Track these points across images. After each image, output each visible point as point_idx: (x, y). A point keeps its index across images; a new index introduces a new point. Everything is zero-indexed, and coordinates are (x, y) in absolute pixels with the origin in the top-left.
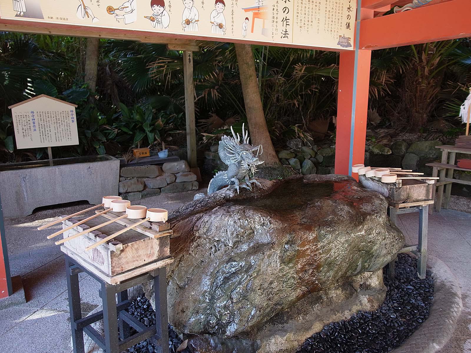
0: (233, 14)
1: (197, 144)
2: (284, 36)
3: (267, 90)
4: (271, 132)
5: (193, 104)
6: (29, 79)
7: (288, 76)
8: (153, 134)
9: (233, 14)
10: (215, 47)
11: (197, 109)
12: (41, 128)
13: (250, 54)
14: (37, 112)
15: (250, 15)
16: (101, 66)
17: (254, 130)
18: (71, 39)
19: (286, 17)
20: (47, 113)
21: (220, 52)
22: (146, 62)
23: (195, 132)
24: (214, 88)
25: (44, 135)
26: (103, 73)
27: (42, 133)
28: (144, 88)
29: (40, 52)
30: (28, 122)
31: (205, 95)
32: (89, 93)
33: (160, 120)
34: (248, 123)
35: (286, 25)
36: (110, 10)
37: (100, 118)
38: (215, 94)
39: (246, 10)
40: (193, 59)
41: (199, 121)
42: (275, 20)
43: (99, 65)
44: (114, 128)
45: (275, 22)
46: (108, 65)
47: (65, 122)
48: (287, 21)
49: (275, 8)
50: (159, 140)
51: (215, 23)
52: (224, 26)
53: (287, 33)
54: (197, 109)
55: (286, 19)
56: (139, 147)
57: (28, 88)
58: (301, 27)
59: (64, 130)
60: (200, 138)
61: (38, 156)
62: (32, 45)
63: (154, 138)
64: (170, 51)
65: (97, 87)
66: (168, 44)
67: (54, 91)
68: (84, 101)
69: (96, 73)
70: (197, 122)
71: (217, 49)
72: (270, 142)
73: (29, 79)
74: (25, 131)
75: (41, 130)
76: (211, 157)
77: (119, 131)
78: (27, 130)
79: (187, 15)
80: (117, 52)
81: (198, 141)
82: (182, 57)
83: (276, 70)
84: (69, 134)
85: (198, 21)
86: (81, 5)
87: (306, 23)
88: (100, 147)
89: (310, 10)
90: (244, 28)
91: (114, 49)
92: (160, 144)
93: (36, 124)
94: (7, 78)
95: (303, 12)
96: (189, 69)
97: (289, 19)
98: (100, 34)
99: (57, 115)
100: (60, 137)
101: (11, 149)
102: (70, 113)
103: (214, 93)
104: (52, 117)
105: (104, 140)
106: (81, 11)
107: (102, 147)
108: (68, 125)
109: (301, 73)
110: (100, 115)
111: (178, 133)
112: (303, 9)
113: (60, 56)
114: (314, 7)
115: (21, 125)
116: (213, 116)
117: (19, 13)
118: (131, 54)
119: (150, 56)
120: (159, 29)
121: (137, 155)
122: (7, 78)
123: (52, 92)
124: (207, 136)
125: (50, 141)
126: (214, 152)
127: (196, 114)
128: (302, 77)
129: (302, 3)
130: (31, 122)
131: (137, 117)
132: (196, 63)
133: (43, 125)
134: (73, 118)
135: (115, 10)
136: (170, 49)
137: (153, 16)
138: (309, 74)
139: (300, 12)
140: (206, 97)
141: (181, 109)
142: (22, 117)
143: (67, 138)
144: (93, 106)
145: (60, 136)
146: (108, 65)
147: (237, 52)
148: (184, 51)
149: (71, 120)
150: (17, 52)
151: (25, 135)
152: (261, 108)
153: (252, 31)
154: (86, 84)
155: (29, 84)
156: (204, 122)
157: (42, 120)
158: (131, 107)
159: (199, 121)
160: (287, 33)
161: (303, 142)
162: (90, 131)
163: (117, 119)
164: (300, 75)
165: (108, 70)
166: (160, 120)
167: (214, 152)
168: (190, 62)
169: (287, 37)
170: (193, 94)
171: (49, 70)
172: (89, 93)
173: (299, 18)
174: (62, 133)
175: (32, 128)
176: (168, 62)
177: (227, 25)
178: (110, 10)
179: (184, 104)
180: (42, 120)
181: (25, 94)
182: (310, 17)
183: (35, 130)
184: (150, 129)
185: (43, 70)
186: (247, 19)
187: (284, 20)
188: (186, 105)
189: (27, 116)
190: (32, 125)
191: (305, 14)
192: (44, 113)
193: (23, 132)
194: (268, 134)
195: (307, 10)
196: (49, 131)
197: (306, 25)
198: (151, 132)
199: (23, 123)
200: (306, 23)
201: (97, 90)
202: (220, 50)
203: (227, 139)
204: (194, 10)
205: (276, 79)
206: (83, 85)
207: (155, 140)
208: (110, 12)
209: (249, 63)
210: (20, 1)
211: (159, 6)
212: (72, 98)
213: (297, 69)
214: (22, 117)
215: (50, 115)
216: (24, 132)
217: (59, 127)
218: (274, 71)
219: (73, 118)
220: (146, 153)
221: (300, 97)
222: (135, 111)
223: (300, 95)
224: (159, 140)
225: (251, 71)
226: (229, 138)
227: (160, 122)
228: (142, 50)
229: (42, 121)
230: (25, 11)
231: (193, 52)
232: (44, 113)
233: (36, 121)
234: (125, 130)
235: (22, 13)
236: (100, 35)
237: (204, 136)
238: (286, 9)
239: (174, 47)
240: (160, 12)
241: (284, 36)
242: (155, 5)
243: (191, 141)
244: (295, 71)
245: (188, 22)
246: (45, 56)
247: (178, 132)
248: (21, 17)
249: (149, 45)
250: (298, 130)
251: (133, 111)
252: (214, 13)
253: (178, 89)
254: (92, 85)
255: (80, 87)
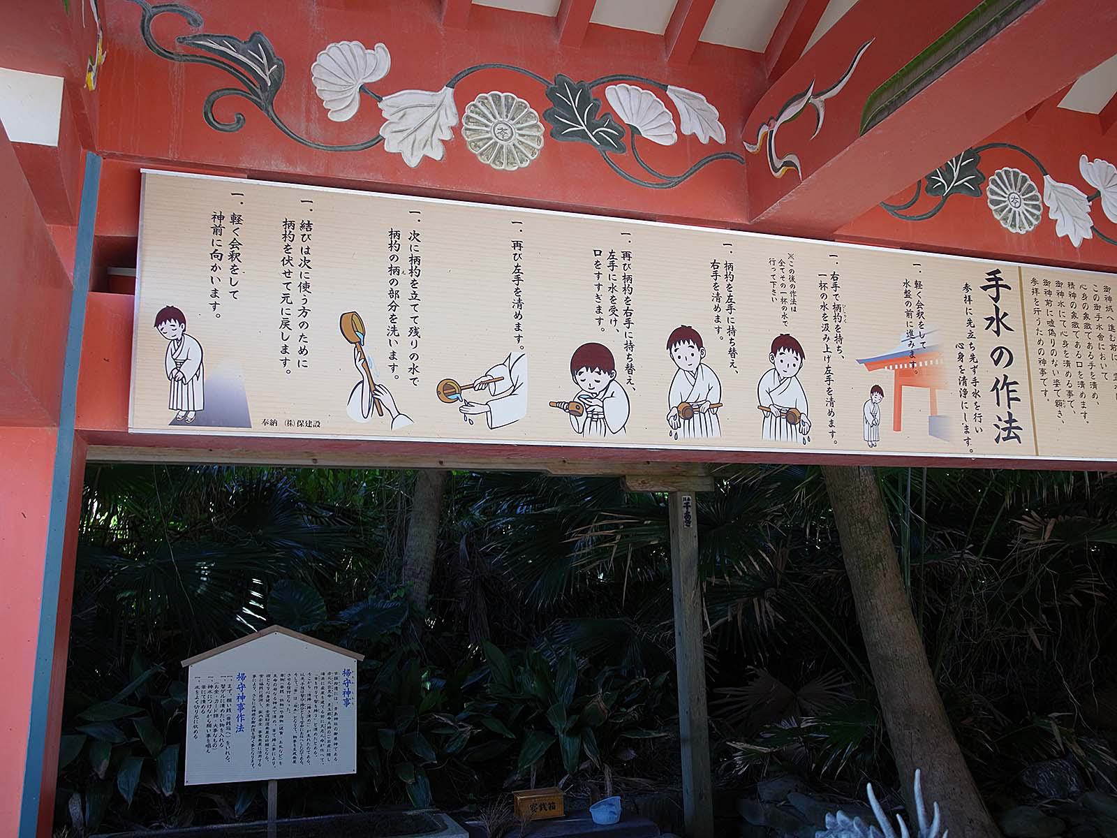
0: (829, 379)
1: (712, 771)
2: (1004, 434)
3: (930, 594)
4: (965, 739)
5: (700, 645)
6: (256, 581)
7: (998, 549)
8: (577, 741)
9: (829, 379)
10: (761, 477)
11: (710, 655)
12: (257, 722)
13: (871, 492)
14: (254, 676)
15: (886, 377)
16: (446, 539)
17: (907, 732)
18: (382, 474)
19: (1006, 377)
20: (279, 678)
21: (776, 489)
22: (566, 527)
23: (706, 733)
24: (760, 593)
25: (263, 743)
26: (450, 557)
27: (257, 738)
28: (560, 596)
29: (300, 510)
30: (226, 703)
31: (735, 617)
32: (407, 613)
33: (599, 699)
34: (880, 708)
35: (1009, 399)
36: (448, 390)
37: (428, 685)
38: (765, 612)
39: (873, 364)
40: (698, 510)
41: (716, 690)
42: (970, 388)
43: (441, 536)
44: (463, 720)
45: (970, 394)
46: (464, 537)
47: (326, 704)
48: (1011, 387)
49: (967, 352)
50: (595, 760)
51: (773, 409)
52: (803, 417)
53: (1014, 424)
54: (710, 655)
55: (1005, 383)
56: (533, 782)
57: (253, 603)
58: (1058, 404)
59: (319, 729)
60: (721, 754)
61: (240, 808)
62: (284, 493)
63: (580, 752)
64: (632, 494)
65: (430, 597)
66: (624, 476)
67: (318, 609)
68: (394, 634)
69: (431, 558)
70: (711, 696)
71: (766, 481)
72: (965, 774)
73: (256, 581)
74: (215, 730)
75: (257, 728)
76: (762, 820)
77: (476, 732)
78: (219, 729)
79: (682, 391)
80: (492, 499)
81: (715, 762)
82: (666, 508)
83: (948, 533)
84: (333, 742)
85: (719, 405)
86: (362, 382)
87: (1076, 390)
88: (416, 783)
89: (1084, 351)
90: (870, 419)
91: (484, 494)
92: (596, 772)
93: (247, 712)
94: (205, 579)
95: (1061, 358)
96: (686, 543)
97: (1015, 383)
98: (442, 460)
99: (306, 686)
100: (305, 750)
101: (167, 784)
102: (342, 678)
103: (763, 610)
104: (292, 689)
105: (432, 758)
106: (362, 398)
107: (424, 781)
108: (332, 714)
109: (1040, 542)
110: (428, 679)
111: (654, 739)
112: (1059, 347)
113: (349, 518)
114: (1095, 341)
115: (206, 714)
116: (758, 677)
117: (182, 414)
118: (528, 505)
119: (576, 508)
120: (594, 438)
121: (526, 811)
122: (205, 579)
123: (313, 611)
124: (746, 752)
125: (277, 761)
126: (768, 802)
127: (707, 669)
128: (1045, 554)
129: (1052, 332)
130: (234, 706)
131: (533, 686)
132: (706, 525)
133: (264, 714)
134: (349, 693)
135: (462, 388)
136: (632, 489)
137: (577, 400)
138: (1068, 545)
139: (1049, 358)
140: (739, 623)
141: (661, 660)
142: (213, 690)
143: (325, 753)
144: (415, 647)
145: (305, 747)
146: (464, 537)
147: (829, 490)
148: (671, 493)
149: (341, 697)
150: (245, 511)
151: (212, 743)
152: (923, 658)
153: (897, 427)
154: (404, 587)
155: (255, 594)
156: (732, 696)
157: (265, 698)
158: (519, 650)
159: (716, 690)
160: (1014, 424)
161: (1081, 772)
162: (391, 732)
163: (475, 689)
164: (1040, 547)
165: (465, 548)
166: (599, 699)
167: (768, 802)
168: (688, 522)
169: (1017, 437)
170: (699, 617)
171: (314, 553)
172: (407, 613)
173: (1050, 378)
174: (312, 738)
175: (235, 724)
176: (627, 525)
177: (817, 416)
178: (448, 390)
179: (672, 642)
180: (265, 698)
181: (239, 618)
182: (1086, 370)
183: (241, 728)
184: (567, 725)
185: (301, 554)
186: (876, 389)
187: (999, 386)
188: (677, 645)
189: (226, 687)
190: (235, 712)
191: (1068, 364)
192: (272, 678)
193: (209, 735)
194: (954, 747)
195: (1072, 350)
196: (278, 731)
197: (1076, 397)
198: (571, 733)
199: (212, 709)
200: (1076, 390)
201: (430, 604)
202: (775, 486)
203: (850, 829)
204: (706, 378)
205: (956, 561)
206: (394, 590)
207: (583, 757)
208: (447, 395)
209: (872, 519)
210: (190, 383)
211: (597, 370)
212: (362, 627)
213: (1026, 529)
214: (213, 690)
215: (286, 686)
216: (212, 733)
217: (305, 719)
218: (942, 537)
219: (349, 693)
220: (552, 806)
221: (1044, 616)
222: (528, 667)
223: (1045, 611)
224: (595, 760)
225: (880, 543)
226: (859, 826)
227: (599, 702)
228: (556, 493)
229: (264, 703)
230: (199, 407)
231: (698, 494)
232: (272, 678)
233: (247, 702)
234: (495, 726)
235: (191, 415)
236: (441, 463)
237: (736, 750)
238: (1001, 353)
239: (643, 482)
240: (598, 388)
241: (1004, 434)
242: (584, 369)
243: (692, 763)
244: (1021, 537)
245: (687, 411)
246: (310, 517)
247: (654, 735)
248: (188, 424)
249: (577, 481)
250: (1062, 734)
251: (522, 668)
252: (769, 381)
253: (653, 596)
254: (420, 590)
255: (387, 597)
